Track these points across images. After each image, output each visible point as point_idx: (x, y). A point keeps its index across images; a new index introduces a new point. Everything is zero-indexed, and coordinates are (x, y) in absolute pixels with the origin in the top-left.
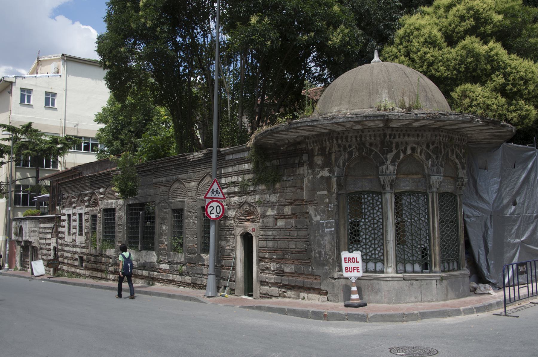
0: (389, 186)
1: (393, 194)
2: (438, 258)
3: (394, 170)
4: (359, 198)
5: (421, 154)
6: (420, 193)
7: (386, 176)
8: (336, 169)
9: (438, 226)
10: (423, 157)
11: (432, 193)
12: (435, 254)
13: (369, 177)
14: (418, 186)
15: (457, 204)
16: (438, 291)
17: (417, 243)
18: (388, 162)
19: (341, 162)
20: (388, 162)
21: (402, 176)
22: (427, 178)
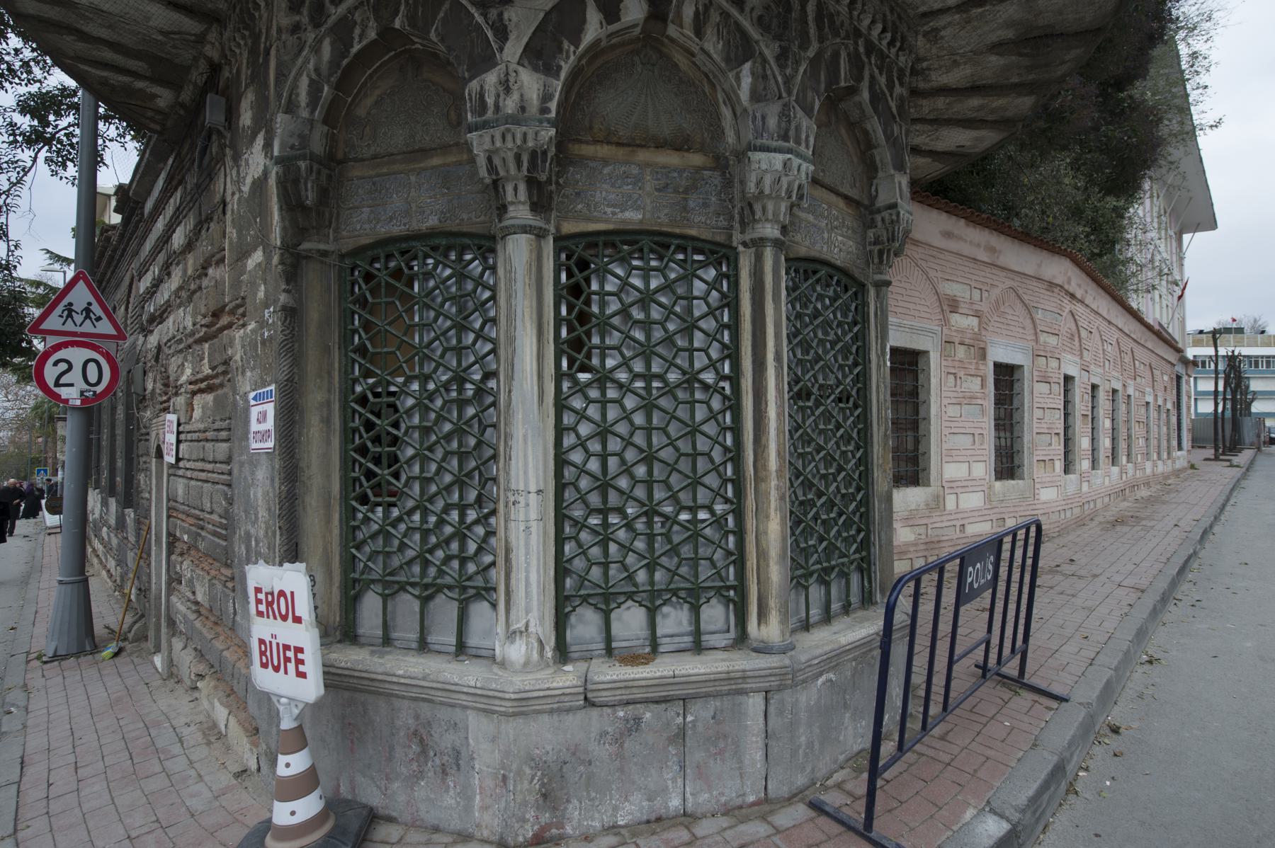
0: (522, 188)
1: (549, 246)
2: (776, 573)
3: (546, 97)
4: (397, 274)
5: (699, 32)
6: (697, 245)
7: (497, 133)
8: (281, 119)
9: (780, 415)
10: (713, 45)
11: (758, 244)
12: (762, 555)
13: (436, 161)
14: (685, 209)
15: (866, 320)
16: (774, 750)
17: (674, 498)
18: (513, 50)
19: (304, 83)
20: (513, 50)
21: (603, 150)
22: (727, 166)
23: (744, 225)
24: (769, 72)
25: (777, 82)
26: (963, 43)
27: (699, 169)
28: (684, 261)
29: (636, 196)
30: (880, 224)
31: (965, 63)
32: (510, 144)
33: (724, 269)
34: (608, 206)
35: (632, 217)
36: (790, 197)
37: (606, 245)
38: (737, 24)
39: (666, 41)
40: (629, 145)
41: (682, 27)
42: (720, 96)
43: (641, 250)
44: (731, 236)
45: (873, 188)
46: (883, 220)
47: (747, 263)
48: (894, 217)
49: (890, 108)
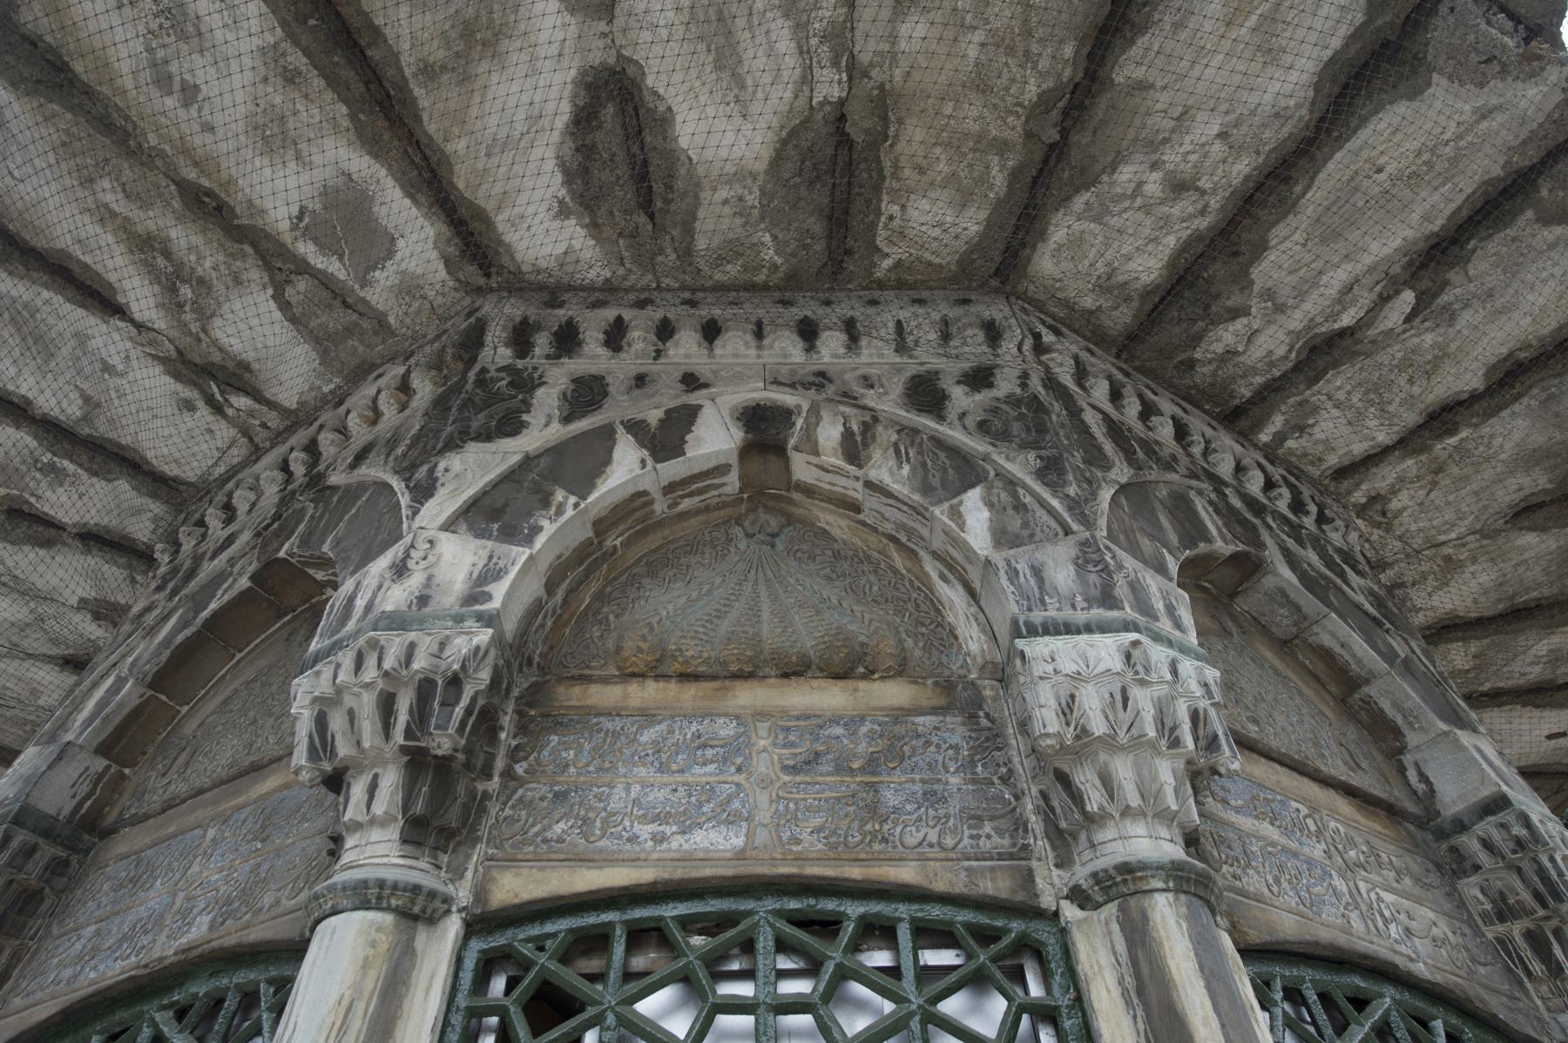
1: (439, 949)
11: (1120, 885)
14: (873, 810)
23: (1063, 843)
24: (1028, 499)
25: (1051, 512)
26: (1449, 515)
27: (900, 714)
28: (894, 972)
29: (728, 789)
30: (1483, 857)
31: (1474, 560)
32: (370, 673)
33: (1035, 990)
34: (644, 819)
35: (715, 845)
36: (1175, 743)
37: (639, 936)
38: (939, 442)
39: (797, 496)
40: (714, 678)
41: (817, 454)
42: (931, 568)
43: (748, 947)
44: (1029, 877)
45: (1412, 775)
46: (1487, 844)
47: (1105, 959)
48: (1518, 830)
49: (1358, 607)
